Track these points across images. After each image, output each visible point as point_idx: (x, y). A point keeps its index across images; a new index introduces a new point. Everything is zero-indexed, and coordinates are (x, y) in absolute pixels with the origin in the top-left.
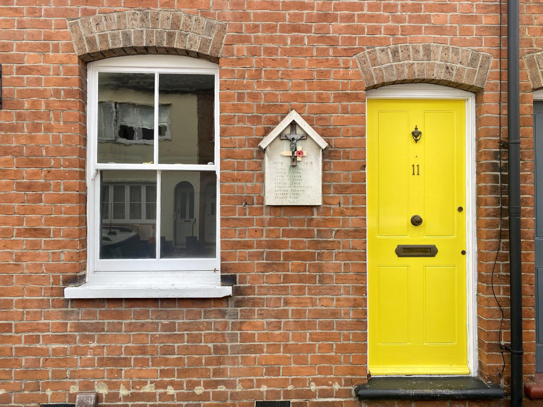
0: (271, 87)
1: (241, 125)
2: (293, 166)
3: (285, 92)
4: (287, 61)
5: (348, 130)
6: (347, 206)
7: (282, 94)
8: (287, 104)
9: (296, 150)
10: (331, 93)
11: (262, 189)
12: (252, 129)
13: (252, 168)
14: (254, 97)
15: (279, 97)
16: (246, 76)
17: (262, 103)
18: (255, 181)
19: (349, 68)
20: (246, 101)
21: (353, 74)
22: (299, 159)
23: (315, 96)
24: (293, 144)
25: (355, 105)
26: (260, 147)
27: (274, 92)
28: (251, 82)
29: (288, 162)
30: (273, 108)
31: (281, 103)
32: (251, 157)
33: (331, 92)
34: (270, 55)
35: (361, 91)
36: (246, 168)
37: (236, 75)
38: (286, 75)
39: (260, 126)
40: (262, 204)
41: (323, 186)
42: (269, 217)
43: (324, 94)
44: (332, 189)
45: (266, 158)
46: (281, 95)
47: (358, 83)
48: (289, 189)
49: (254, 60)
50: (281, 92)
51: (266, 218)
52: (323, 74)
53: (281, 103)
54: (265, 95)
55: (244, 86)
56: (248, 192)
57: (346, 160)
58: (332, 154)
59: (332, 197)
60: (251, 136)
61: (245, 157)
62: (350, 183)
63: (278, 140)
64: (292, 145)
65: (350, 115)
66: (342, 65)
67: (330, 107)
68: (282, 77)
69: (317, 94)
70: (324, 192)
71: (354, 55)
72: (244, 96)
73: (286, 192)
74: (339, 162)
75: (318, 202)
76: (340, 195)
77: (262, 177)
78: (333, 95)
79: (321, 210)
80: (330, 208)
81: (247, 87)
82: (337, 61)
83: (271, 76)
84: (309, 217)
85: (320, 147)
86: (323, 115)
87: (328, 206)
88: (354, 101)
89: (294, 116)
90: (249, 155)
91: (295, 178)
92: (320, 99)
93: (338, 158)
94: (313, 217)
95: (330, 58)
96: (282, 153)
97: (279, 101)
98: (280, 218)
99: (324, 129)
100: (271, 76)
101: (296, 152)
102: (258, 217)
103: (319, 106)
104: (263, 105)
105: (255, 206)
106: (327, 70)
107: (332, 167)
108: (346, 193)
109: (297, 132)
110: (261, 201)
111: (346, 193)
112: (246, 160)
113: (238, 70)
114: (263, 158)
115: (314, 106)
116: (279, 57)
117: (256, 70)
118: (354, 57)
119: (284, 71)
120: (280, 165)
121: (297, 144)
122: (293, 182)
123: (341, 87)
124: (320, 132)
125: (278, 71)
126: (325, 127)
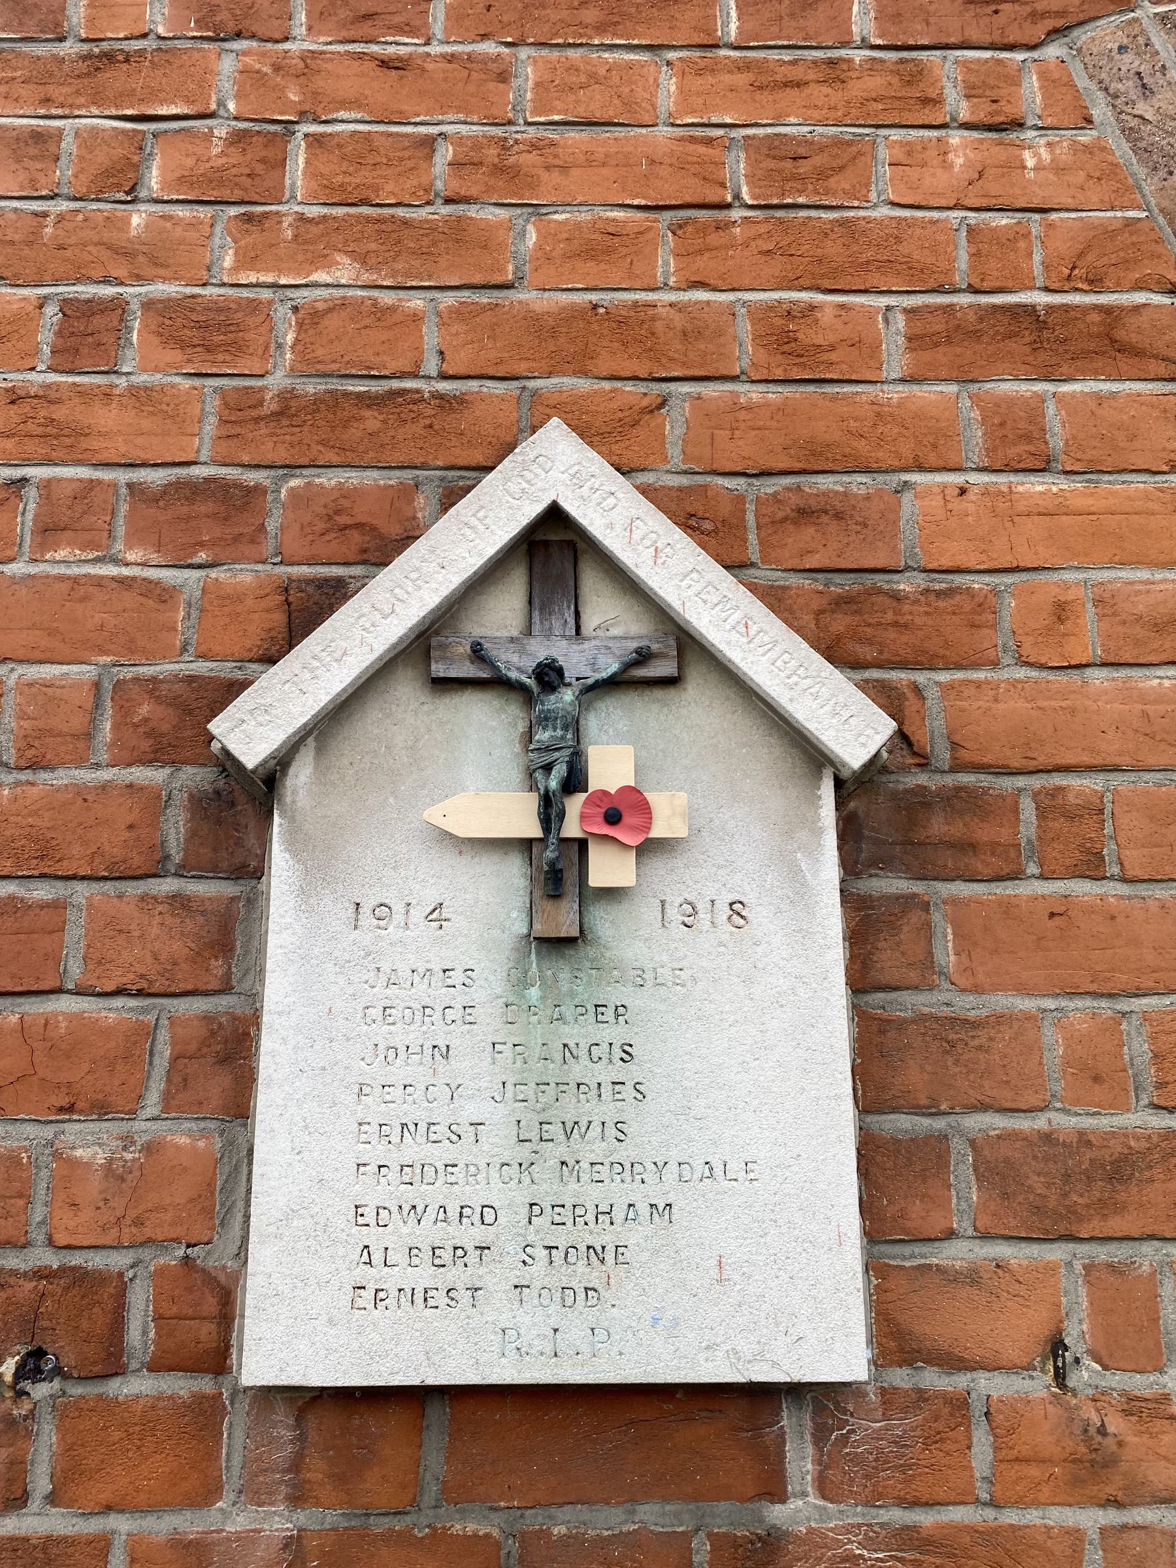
0: (363, 259)
1: (66, 561)
2: (556, 946)
3: (484, 298)
4: (503, 77)
5: (1061, 611)
6: (1140, 1384)
7: (460, 313)
8: (498, 388)
9: (575, 781)
10: (887, 314)
11: (222, 1190)
12: (164, 595)
13: (132, 961)
14: (209, 332)
15: (431, 337)
16: (154, 180)
17: (277, 381)
18: (152, 1102)
19: (1019, 125)
20: (139, 363)
21: (1059, 169)
22: (607, 868)
23: (744, 328)
24: (545, 720)
25: (1099, 398)
26: (227, 763)
27: (387, 298)
28: (193, 224)
29: (498, 899)
30: (372, 420)
31: (444, 386)
32: (137, 861)
33: (884, 301)
34: (366, 29)
35: (1140, 298)
36: (75, 970)
37: (64, 172)
38: (498, 171)
39: (242, 576)
40: (218, 1358)
41: (870, 1153)
42: (279, 1522)
43: (826, 317)
44: (965, 1190)
45: (281, 863)
46: (445, 319)
47: (1109, 233)
48: (509, 1196)
49: (227, 65)
50: (448, 299)
51: (249, 1538)
52: (804, 167)
53: (444, 386)
54: (310, 320)
55: (125, 253)
56: (67, 1226)
57: (1082, 888)
58: (938, 826)
59: (971, 1277)
60: (151, 658)
61: (76, 860)
62: (1141, 1120)
63: (406, 692)
64: (543, 736)
65: (1061, 484)
66: (958, 105)
67: (881, 414)
68: (457, 187)
69: (761, 314)
70: (879, 1223)
71: (1055, 33)
72: (120, 331)
73: (471, 1234)
74: (1007, 907)
75: (833, 1346)
76: (1057, 1253)
77: (227, 1060)
78: (900, 321)
79: (866, 1429)
80: (959, 1404)
81: (146, 258)
82: (914, 75)
83: (365, 176)
84: (726, 1517)
85: (811, 755)
86: (826, 482)
87: (933, 1379)
88: (1095, 374)
89: (556, 470)
90: (114, 843)
91: (579, 1070)
92: (792, 350)
93: (997, 864)
94: (777, 1514)
95: (858, 56)
96: (435, 815)
97: (431, 366)
98: (404, 1539)
99: (843, 602)
100: (365, 176)
101: (575, 805)
102: (162, 1526)
103: (781, 410)
104: (287, 397)
105: (136, 1386)
106: (839, 143)
107: (946, 953)
108: (1117, 1225)
109: (591, 620)
110: (207, 1331)
111: (1117, 1225)
112: (81, 892)
113: (88, 140)
114: (251, 870)
115: (736, 407)
116: (435, 49)
117: (238, 139)
118: (1053, 51)
119: (477, 144)
120: (422, 930)
121: (592, 723)
122: (557, 1117)
123: (963, 260)
124: (807, 619)
125: (428, 144)
126: (843, 584)
